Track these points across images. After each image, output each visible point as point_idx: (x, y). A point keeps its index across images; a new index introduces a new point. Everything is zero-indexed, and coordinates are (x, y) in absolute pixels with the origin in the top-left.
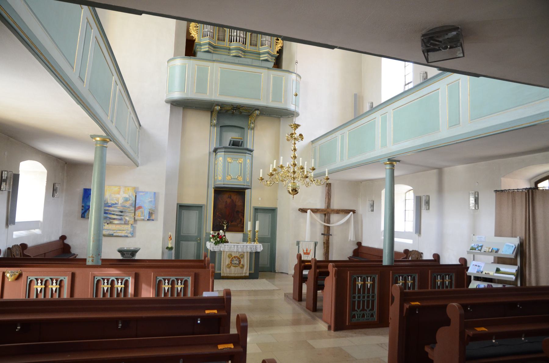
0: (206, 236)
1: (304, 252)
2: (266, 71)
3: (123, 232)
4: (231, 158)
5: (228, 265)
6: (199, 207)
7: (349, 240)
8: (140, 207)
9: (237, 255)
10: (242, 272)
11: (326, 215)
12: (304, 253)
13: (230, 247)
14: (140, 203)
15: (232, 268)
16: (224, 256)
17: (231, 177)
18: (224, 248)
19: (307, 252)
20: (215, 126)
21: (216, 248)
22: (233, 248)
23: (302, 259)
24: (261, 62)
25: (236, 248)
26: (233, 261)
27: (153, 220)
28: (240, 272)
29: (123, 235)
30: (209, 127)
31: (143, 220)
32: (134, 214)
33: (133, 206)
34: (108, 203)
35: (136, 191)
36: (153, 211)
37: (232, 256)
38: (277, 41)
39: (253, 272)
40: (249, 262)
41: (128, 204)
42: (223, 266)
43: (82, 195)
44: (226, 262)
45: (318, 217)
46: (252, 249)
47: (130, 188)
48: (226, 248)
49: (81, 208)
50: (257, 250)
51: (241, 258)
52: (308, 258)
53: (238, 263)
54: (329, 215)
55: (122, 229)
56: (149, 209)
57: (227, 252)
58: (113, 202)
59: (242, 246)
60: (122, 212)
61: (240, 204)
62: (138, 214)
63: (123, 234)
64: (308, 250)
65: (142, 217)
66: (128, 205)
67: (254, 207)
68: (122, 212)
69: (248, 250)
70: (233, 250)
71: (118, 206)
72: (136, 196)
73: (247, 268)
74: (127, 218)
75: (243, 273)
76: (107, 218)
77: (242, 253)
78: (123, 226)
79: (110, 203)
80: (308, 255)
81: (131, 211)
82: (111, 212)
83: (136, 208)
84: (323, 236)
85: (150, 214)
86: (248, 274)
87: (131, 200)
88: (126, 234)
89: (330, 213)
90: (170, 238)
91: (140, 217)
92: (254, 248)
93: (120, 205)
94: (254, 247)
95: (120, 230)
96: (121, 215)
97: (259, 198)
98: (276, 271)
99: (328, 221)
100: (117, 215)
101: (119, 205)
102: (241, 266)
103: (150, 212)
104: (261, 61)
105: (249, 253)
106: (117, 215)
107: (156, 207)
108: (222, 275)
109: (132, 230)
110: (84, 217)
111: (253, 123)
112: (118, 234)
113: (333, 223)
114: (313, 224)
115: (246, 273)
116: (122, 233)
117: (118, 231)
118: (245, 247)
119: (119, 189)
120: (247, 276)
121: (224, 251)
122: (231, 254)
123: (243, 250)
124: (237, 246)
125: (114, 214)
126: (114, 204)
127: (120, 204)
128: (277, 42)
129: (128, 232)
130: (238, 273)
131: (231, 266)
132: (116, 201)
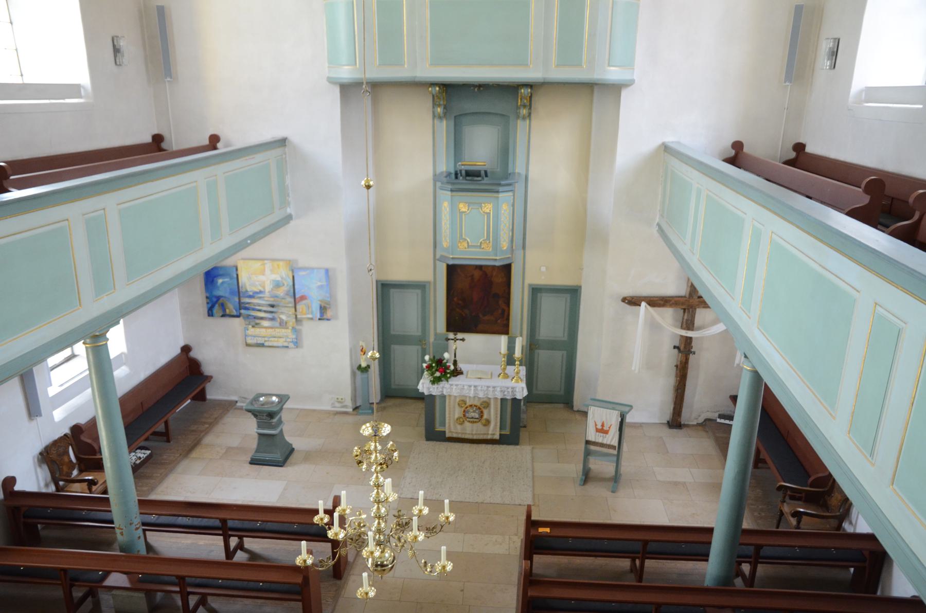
0: (435, 339)
1: (597, 427)
3: (280, 340)
4: (466, 203)
6: (421, 287)
7: (735, 365)
8: (303, 298)
10: (486, 433)
11: (687, 311)
12: (597, 429)
15: (467, 425)
16: (449, 402)
17: (468, 243)
18: (449, 390)
19: (602, 429)
20: (440, 118)
21: (435, 390)
23: (533, 518)
26: (468, 412)
27: (328, 320)
28: (482, 433)
29: (280, 344)
30: (431, 121)
31: (312, 319)
32: (294, 309)
34: (247, 291)
35: (294, 269)
36: (327, 304)
37: (465, 404)
39: (507, 432)
41: (281, 292)
42: (450, 420)
44: (454, 414)
45: (667, 318)
46: (506, 393)
47: (281, 263)
48: (454, 390)
49: (205, 301)
50: (515, 395)
51: (484, 407)
53: (477, 416)
54: (692, 311)
57: (455, 397)
58: (255, 290)
59: (486, 388)
60: (273, 306)
61: (501, 280)
62: (301, 310)
63: (281, 342)
65: (308, 314)
67: (530, 285)
68: (273, 306)
69: (496, 395)
70: (468, 393)
72: (293, 277)
73: (496, 425)
74: (284, 317)
75: (488, 434)
76: (250, 317)
77: (485, 400)
78: (278, 330)
79: (251, 291)
80: (605, 435)
82: (255, 306)
83: (296, 299)
84: (676, 350)
85: (323, 309)
86: (497, 437)
88: (286, 344)
89: (695, 309)
90: (362, 351)
91: (305, 314)
92: (508, 392)
94: (510, 390)
95: (275, 337)
96: (272, 312)
97: (542, 268)
98: (575, 408)
99: (689, 325)
100: (265, 311)
101: (267, 294)
103: (322, 306)
106: (265, 311)
108: (448, 435)
109: (294, 337)
110: (212, 315)
111: (525, 106)
113: (699, 328)
114: (653, 326)
115: (494, 434)
116: (278, 341)
117: (273, 339)
118: (491, 389)
119: (261, 265)
121: (450, 396)
122: (462, 401)
123: (487, 394)
124: (475, 386)
125: (260, 310)
126: (257, 293)
129: (288, 340)
130: (479, 434)
131: (464, 421)
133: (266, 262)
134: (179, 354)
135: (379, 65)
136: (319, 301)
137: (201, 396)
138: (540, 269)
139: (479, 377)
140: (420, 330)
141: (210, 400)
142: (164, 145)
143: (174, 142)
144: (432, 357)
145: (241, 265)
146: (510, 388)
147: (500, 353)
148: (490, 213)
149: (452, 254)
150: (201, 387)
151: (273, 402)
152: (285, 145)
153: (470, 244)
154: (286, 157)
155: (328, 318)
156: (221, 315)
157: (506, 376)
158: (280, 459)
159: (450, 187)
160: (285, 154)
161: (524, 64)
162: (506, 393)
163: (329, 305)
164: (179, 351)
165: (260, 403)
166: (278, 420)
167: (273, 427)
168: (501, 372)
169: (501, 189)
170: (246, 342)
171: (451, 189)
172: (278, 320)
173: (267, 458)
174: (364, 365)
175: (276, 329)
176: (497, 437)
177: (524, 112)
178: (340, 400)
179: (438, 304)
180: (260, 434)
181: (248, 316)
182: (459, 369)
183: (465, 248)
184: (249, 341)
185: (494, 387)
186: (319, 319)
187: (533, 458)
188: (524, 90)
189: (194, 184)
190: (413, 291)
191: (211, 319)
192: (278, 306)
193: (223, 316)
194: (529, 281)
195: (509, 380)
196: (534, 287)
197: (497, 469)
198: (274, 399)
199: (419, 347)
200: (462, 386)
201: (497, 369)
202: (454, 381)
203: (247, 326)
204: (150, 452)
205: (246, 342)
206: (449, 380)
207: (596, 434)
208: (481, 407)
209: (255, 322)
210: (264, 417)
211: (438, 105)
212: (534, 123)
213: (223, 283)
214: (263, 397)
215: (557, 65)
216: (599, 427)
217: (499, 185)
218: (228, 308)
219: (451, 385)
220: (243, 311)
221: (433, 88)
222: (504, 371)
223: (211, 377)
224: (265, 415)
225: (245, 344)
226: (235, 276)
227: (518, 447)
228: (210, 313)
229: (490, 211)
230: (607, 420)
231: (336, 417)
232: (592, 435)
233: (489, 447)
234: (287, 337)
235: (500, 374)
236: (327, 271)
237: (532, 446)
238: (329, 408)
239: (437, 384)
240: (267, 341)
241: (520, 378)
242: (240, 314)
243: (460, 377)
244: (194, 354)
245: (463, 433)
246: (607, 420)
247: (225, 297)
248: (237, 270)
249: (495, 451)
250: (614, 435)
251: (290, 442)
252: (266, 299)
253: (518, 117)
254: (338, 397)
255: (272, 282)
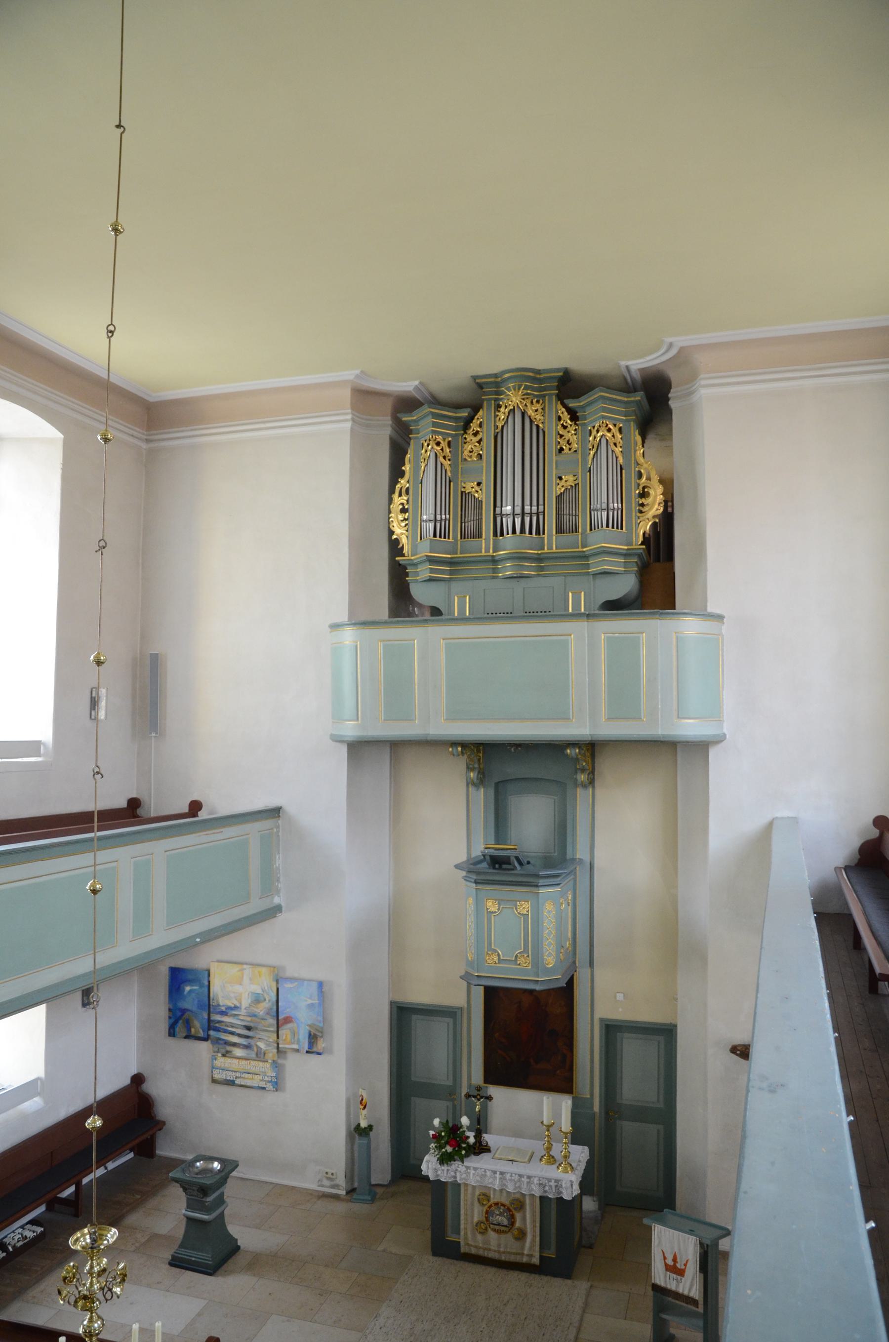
2: (582, 626)
4: (496, 900)
5: (479, 1223)
6: (450, 1013)
8: (288, 1020)
9: (504, 1200)
10: (519, 1251)
12: (666, 1265)
13: (482, 1175)
14: (288, 1010)
15: (492, 1235)
17: (499, 955)
18: (464, 1176)
22: (491, 1177)
24: (594, 579)
25: (498, 1179)
26: (493, 1214)
27: (319, 1054)
28: (514, 1251)
29: (255, 1084)
31: (297, 1051)
32: (275, 1035)
33: (273, 1016)
34: (219, 1005)
36: (319, 1031)
37: (489, 1201)
38: (643, 501)
40: (538, 1225)
41: (261, 1009)
42: (466, 1224)
43: (168, 984)
44: (473, 1217)
46: (547, 1188)
47: (264, 970)
48: (471, 1175)
50: (561, 1192)
52: (681, 1285)
55: (253, 1070)
56: (307, 1025)
57: (474, 1187)
60: (249, 1028)
62: (284, 1037)
63: (256, 1081)
64: (678, 1260)
65: (293, 1043)
66: (261, 1013)
67: (602, 1020)
68: (249, 1028)
69: (532, 1189)
70: (491, 1183)
71: (240, 1014)
72: (278, 989)
73: (533, 1241)
74: (262, 1045)
75: (523, 1254)
77: (518, 1196)
78: (253, 1063)
79: (223, 1006)
80: (679, 1277)
81: (268, 1027)
82: (228, 1026)
83: (280, 1021)
85: (313, 1038)
87: (267, 1001)
88: (262, 1084)
91: (288, 1044)
92: (551, 1186)
93: (245, 1011)
94: (553, 1184)
95: (249, 1073)
96: (247, 1037)
101: (243, 1012)
102: (516, 1232)
103: (312, 1034)
104: (591, 576)
105: (538, 1200)
106: (240, 1035)
107: (326, 1018)
109: (274, 1074)
110: (174, 1036)
111: (583, 770)
112: (246, 1081)
117: (246, 1075)
119: (239, 971)
120: (534, 1266)
121: (466, 1185)
122: (484, 1195)
124: (502, 1173)
125: (232, 1033)
127: (245, 1009)
128: (642, 505)
129: (266, 1079)
131: (486, 1229)
132: (236, 1000)
133: (245, 966)
134: (129, 1085)
135: (384, 720)
136: (309, 1026)
137: (146, 1149)
138: (615, 997)
139: (511, 1159)
140: (451, 1078)
141: (160, 1157)
142: (140, 811)
143: (152, 808)
144: (445, 1121)
145: (215, 969)
146: (553, 1181)
147: (542, 1123)
148: (528, 915)
149: (477, 972)
150: (147, 1135)
151: (211, 1170)
152: (279, 816)
153: (502, 958)
154: (278, 832)
155: (318, 1051)
156: (184, 1035)
157: (552, 1160)
158: (210, 1262)
159: (474, 877)
160: (278, 827)
161: (565, 718)
162: (547, 1188)
163: (322, 1032)
164: (128, 1081)
165: (196, 1170)
166: (215, 1200)
167: (208, 1210)
168: (544, 1153)
169: (541, 882)
170: (212, 1077)
171: (475, 880)
172: (255, 1049)
173: (193, 1259)
174: (364, 1124)
175: (252, 1062)
176: (536, 1260)
177: (582, 777)
178: (329, 1175)
179: (473, 1040)
180: (189, 1219)
181: (217, 1041)
182: (484, 1143)
183: (496, 963)
184: (218, 1075)
185: (529, 1177)
186: (307, 1052)
187: (586, 1304)
188: (570, 750)
189: (114, 864)
190: (440, 1019)
191: (171, 1041)
192: (256, 1029)
193: (187, 1037)
194: (598, 1015)
195: (555, 1166)
196: (609, 1023)
197: (523, 1317)
198: (216, 1165)
199: (450, 1104)
200: (483, 1170)
201: (539, 1147)
202: (473, 1162)
203: (214, 1054)
204: (42, 1229)
205: (212, 1077)
206: (465, 1159)
207: (665, 1276)
208: (511, 1208)
209: (225, 1048)
210: (195, 1193)
211: (471, 768)
212: (598, 792)
213: (190, 991)
214: (202, 1162)
215: (608, 719)
216: (670, 1262)
217: (537, 876)
218: (194, 1027)
219: (468, 1168)
220: (212, 1033)
221: (455, 749)
222: (548, 1152)
223: (164, 1123)
224: (195, 1189)
225: (211, 1080)
226: (207, 983)
227: (569, 1282)
228: (172, 1033)
229: (528, 911)
230: (679, 1249)
231: (320, 1202)
232: (660, 1276)
233: (524, 1276)
234: (265, 1074)
235: (542, 1157)
236: (321, 984)
237: (589, 1284)
238: (313, 1186)
239: (447, 1164)
240: (239, 1077)
241: (571, 1165)
242: (209, 1036)
243: (485, 1156)
244: (151, 1088)
245: (485, 1249)
246: (679, 1249)
247: (192, 1012)
248: (209, 975)
249: (531, 1286)
250: (693, 1279)
251: (235, 1236)
252: (241, 1018)
253: (576, 784)
254: (327, 1170)
255: (250, 994)
